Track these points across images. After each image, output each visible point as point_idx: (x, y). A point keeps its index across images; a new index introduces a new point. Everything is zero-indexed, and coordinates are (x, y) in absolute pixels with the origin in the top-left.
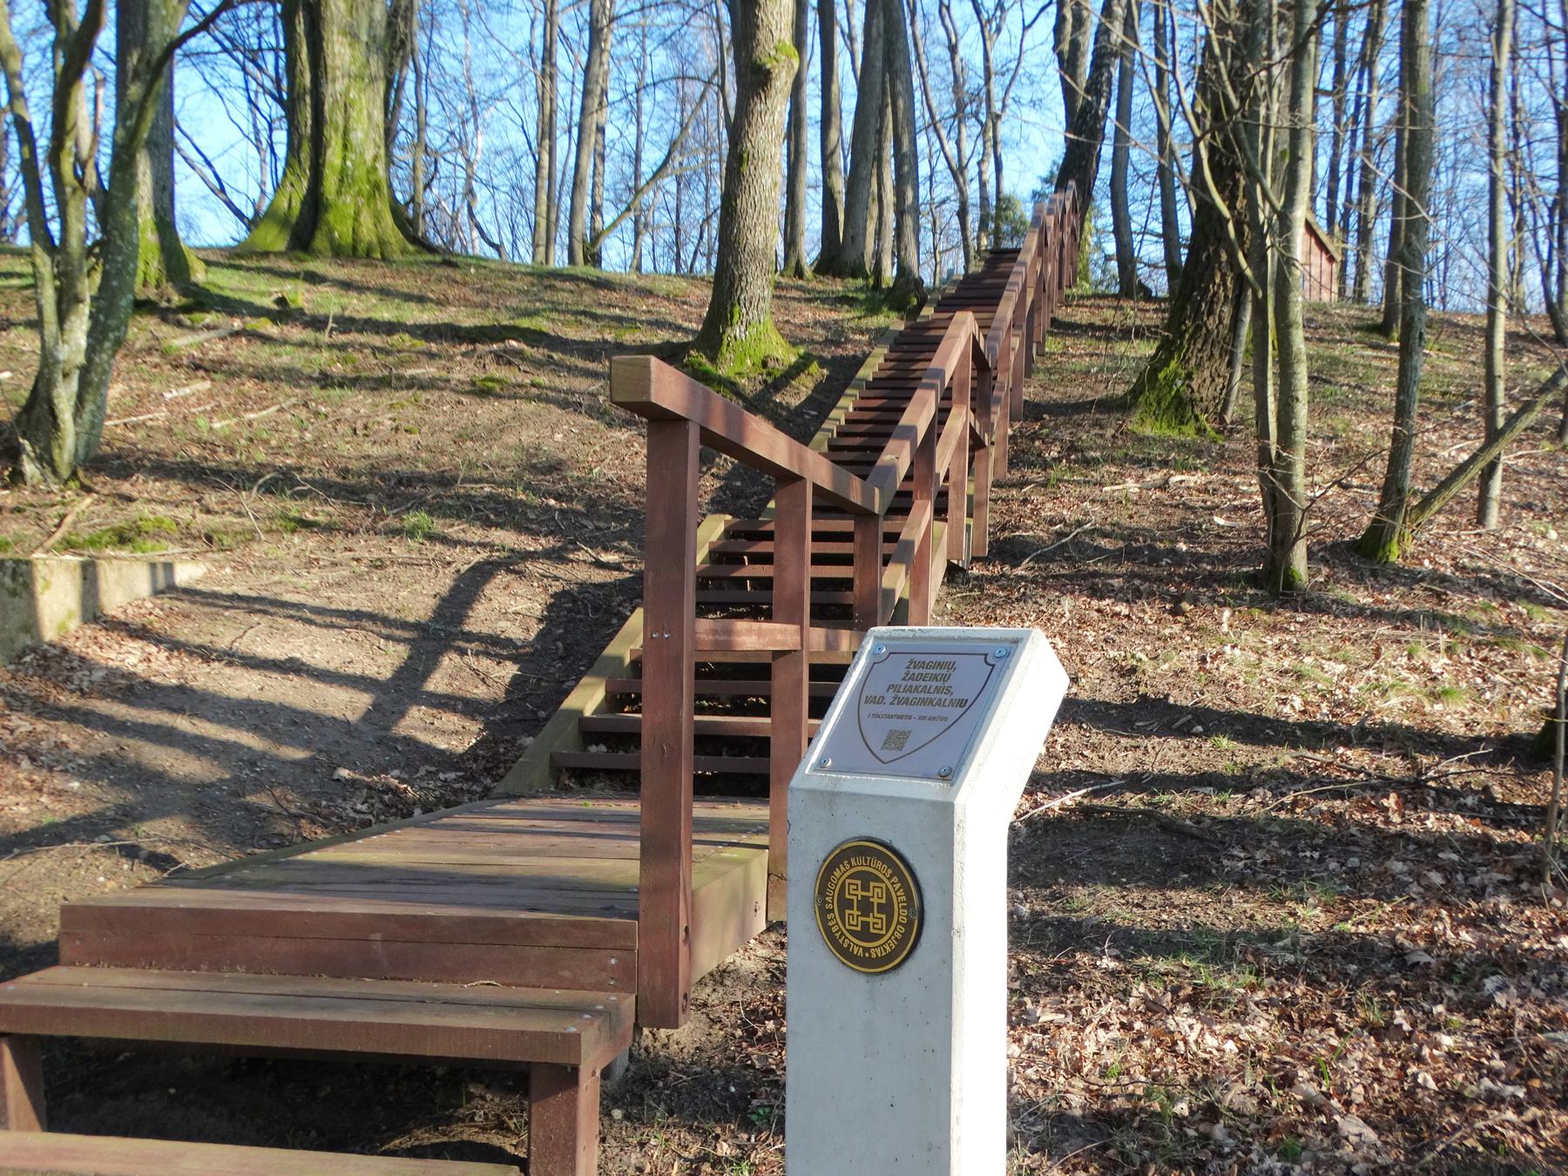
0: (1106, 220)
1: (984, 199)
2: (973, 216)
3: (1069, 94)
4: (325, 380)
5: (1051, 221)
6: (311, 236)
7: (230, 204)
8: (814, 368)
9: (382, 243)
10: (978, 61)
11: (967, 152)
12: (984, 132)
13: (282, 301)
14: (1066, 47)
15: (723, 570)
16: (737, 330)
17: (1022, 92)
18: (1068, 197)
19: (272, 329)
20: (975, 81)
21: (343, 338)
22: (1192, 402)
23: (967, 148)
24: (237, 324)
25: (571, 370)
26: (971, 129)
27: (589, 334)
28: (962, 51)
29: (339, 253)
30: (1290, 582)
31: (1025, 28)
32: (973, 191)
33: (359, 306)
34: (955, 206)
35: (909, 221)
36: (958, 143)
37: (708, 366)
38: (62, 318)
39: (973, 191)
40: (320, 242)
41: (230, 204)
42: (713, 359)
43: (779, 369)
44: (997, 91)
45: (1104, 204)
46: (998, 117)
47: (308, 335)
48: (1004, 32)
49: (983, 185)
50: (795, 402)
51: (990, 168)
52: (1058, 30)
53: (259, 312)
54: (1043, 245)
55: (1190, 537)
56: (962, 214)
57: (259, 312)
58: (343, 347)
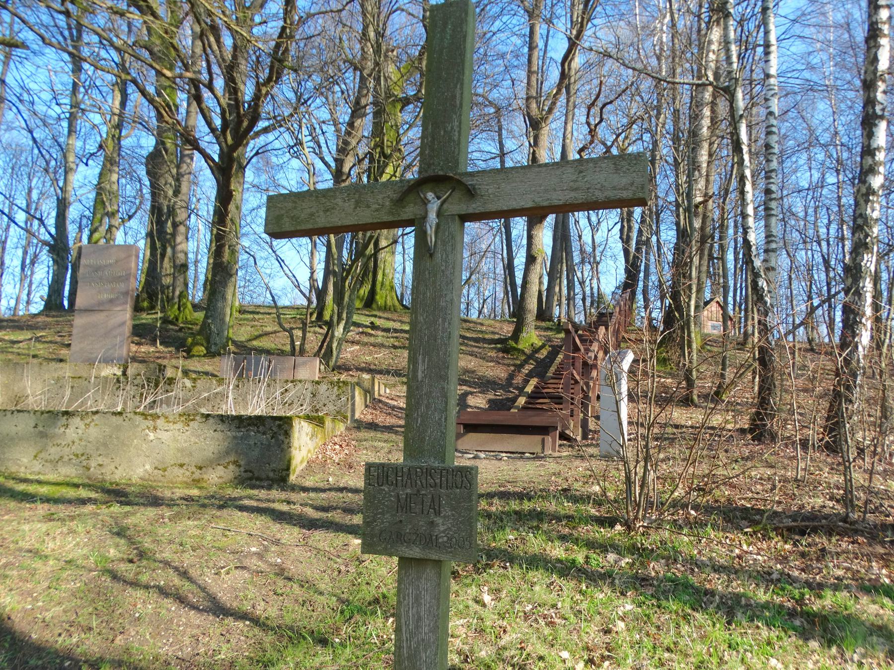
0: (641, 303)
1: (592, 294)
2: (588, 301)
3: (626, 252)
4: (395, 347)
5: (622, 303)
6: (372, 303)
7: (301, 292)
8: (547, 347)
9: (394, 306)
10: (590, 241)
11: (586, 276)
12: (592, 268)
13: (372, 323)
14: (625, 237)
15: (538, 390)
16: (524, 335)
17: (608, 253)
18: (627, 295)
19: (369, 331)
20: (589, 249)
21: (395, 335)
22: (669, 360)
23: (586, 274)
24: (361, 330)
25: (472, 346)
26: (587, 267)
27: (474, 336)
28: (583, 237)
29: (379, 309)
30: (692, 401)
31: (609, 231)
32: (588, 290)
33: (390, 325)
34: (581, 297)
35: (572, 302)
36: (582, 272)
37: (515, 345)
38: (338, 323)
39: (588, 290)
40: (374, 306)
41: (301, 292)
42: (516, 343)
43: (537, 347)
44: (598, 254)
45: (640, 297)
46: (598, 263)
47: (385, 334)
48: (600, 231)
49: (592, 289)
50: (542, 357)
51: (595, 281)
52: (622, 230)
53: (367, 327)
54: (620, 310)
55: (665, 393)
56: (584, 300)
57: (367, 327)
58: (397, 337)
